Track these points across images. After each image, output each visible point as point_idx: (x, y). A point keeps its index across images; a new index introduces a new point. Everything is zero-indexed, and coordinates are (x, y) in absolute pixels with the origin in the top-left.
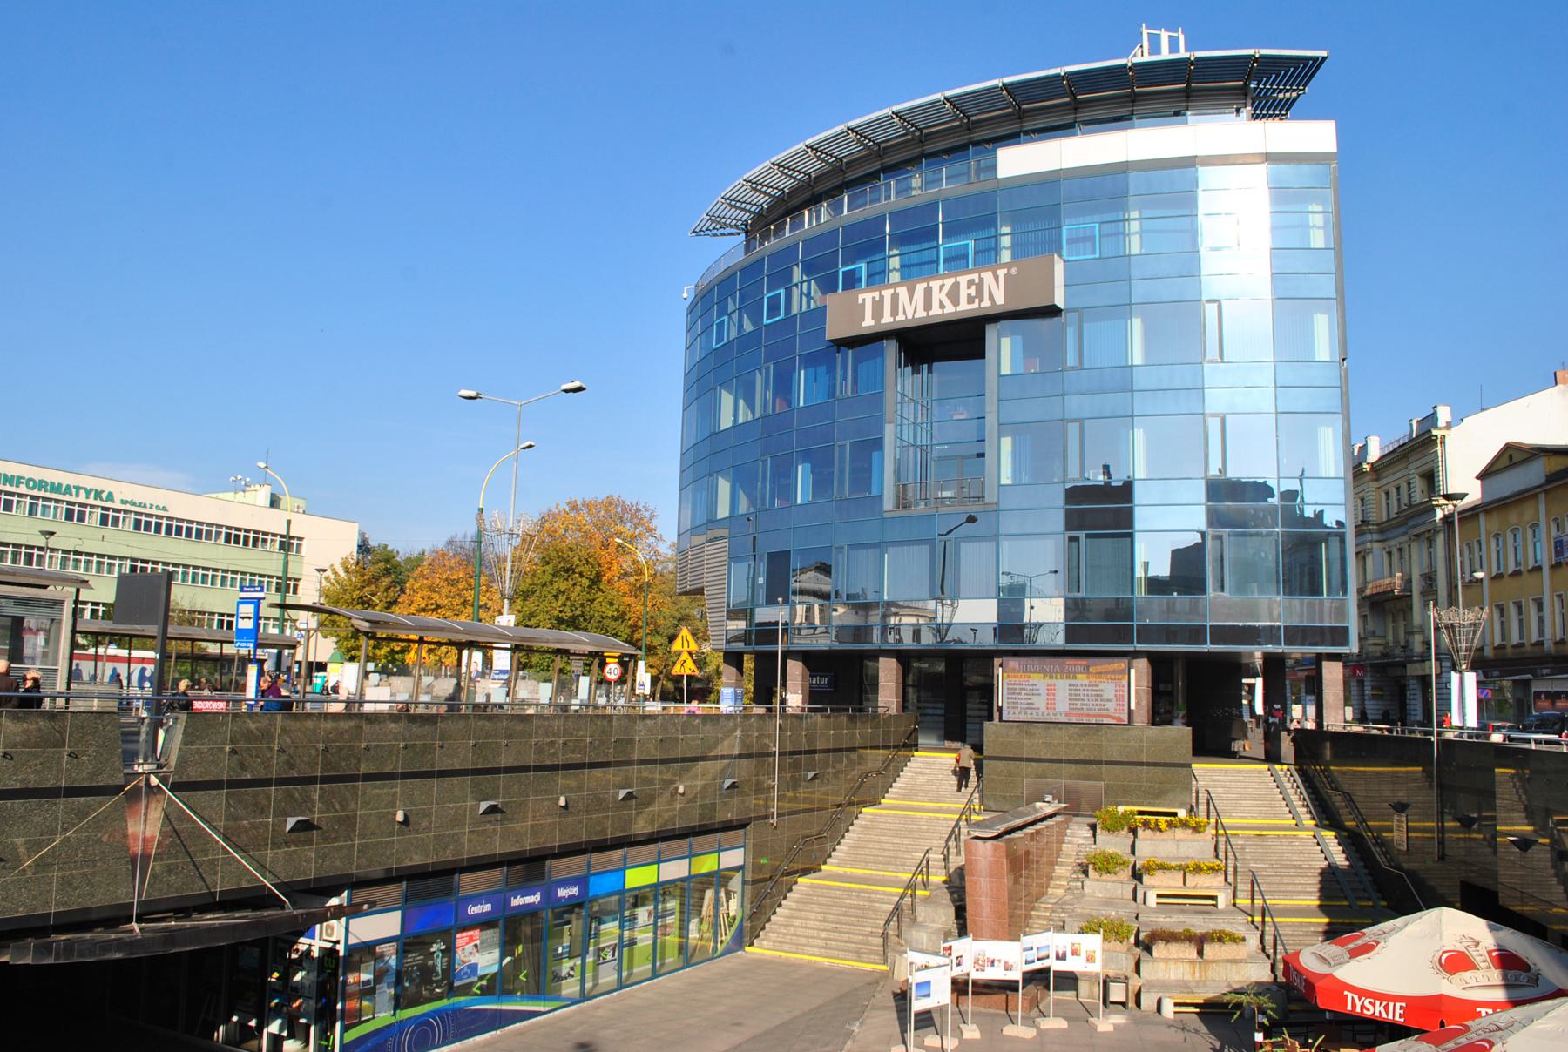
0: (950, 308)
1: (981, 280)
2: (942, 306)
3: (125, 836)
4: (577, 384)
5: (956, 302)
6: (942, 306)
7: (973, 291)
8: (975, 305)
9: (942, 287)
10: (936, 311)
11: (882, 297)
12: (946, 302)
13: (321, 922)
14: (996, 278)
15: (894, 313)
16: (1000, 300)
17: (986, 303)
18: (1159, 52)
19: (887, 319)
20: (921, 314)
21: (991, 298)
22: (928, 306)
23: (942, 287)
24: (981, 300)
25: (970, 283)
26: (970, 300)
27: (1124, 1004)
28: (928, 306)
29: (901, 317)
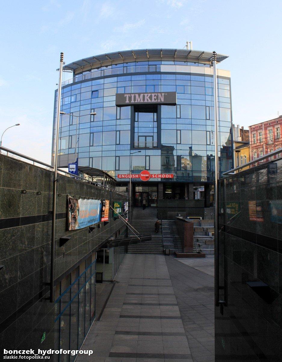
0: (150, 101)
1: (158, 95)
2: (148, 100)
3: (248, 206)
4: (122, 319)
5: (151, 100)
6: (148, 100)
7: (156, 97)
8: (156, 101)
9: (147, 95)
10: (146, 101)
11: (131, 96)
12: (149, 99)
13: (249, 218)
14: (160, 100)
15: (135, 100)
16: (163, 100)
17: (159, 101)
18: (105, 250)
19: (133, 101)
20: (142, 101)
21: (160, 100)
22: (144, 100)
23: (147, 95)
24: (158, 100)
25: (155, 96)
26: (155, 99)
27: (127, 237)
28: (144, 100)
29: (136, 101)
